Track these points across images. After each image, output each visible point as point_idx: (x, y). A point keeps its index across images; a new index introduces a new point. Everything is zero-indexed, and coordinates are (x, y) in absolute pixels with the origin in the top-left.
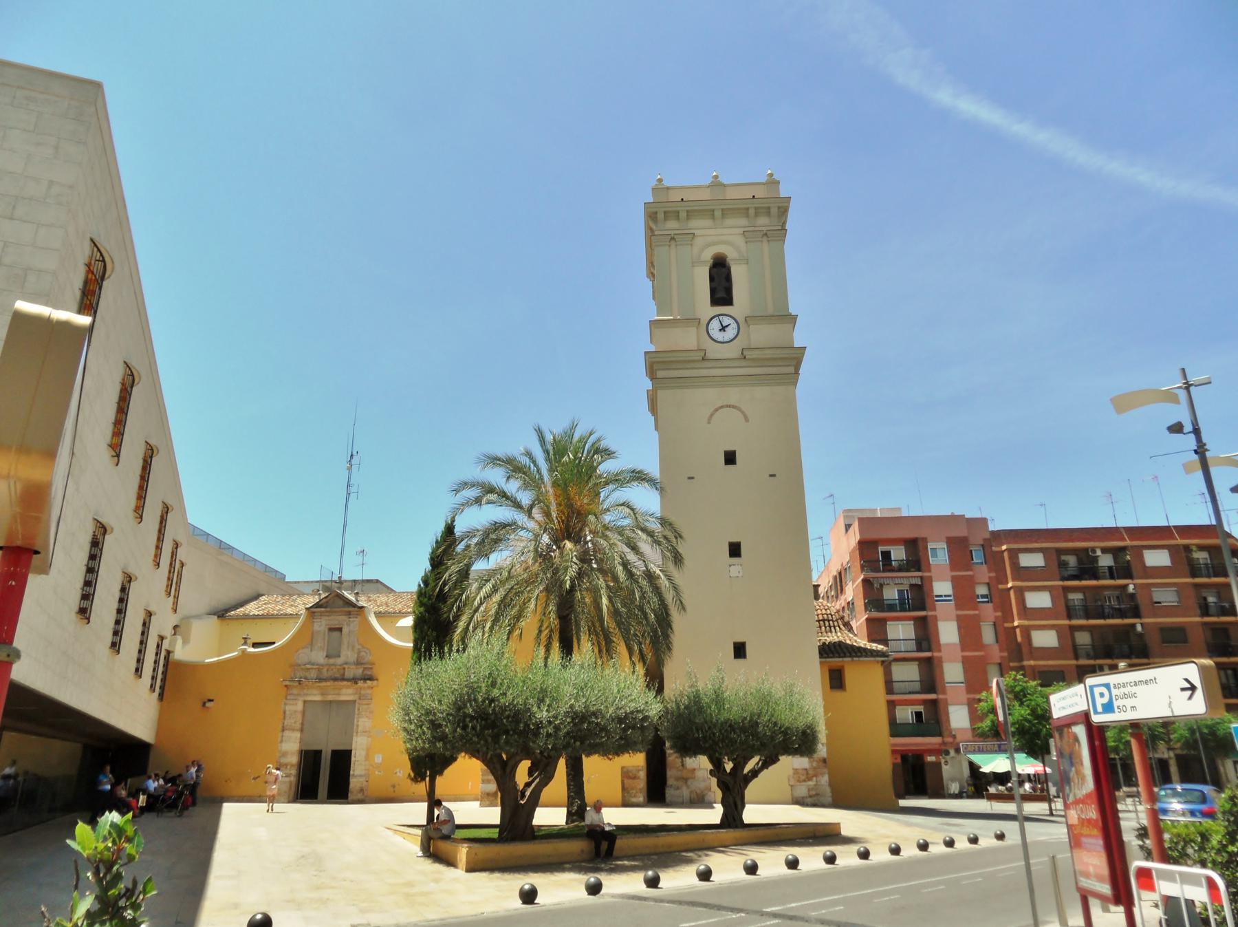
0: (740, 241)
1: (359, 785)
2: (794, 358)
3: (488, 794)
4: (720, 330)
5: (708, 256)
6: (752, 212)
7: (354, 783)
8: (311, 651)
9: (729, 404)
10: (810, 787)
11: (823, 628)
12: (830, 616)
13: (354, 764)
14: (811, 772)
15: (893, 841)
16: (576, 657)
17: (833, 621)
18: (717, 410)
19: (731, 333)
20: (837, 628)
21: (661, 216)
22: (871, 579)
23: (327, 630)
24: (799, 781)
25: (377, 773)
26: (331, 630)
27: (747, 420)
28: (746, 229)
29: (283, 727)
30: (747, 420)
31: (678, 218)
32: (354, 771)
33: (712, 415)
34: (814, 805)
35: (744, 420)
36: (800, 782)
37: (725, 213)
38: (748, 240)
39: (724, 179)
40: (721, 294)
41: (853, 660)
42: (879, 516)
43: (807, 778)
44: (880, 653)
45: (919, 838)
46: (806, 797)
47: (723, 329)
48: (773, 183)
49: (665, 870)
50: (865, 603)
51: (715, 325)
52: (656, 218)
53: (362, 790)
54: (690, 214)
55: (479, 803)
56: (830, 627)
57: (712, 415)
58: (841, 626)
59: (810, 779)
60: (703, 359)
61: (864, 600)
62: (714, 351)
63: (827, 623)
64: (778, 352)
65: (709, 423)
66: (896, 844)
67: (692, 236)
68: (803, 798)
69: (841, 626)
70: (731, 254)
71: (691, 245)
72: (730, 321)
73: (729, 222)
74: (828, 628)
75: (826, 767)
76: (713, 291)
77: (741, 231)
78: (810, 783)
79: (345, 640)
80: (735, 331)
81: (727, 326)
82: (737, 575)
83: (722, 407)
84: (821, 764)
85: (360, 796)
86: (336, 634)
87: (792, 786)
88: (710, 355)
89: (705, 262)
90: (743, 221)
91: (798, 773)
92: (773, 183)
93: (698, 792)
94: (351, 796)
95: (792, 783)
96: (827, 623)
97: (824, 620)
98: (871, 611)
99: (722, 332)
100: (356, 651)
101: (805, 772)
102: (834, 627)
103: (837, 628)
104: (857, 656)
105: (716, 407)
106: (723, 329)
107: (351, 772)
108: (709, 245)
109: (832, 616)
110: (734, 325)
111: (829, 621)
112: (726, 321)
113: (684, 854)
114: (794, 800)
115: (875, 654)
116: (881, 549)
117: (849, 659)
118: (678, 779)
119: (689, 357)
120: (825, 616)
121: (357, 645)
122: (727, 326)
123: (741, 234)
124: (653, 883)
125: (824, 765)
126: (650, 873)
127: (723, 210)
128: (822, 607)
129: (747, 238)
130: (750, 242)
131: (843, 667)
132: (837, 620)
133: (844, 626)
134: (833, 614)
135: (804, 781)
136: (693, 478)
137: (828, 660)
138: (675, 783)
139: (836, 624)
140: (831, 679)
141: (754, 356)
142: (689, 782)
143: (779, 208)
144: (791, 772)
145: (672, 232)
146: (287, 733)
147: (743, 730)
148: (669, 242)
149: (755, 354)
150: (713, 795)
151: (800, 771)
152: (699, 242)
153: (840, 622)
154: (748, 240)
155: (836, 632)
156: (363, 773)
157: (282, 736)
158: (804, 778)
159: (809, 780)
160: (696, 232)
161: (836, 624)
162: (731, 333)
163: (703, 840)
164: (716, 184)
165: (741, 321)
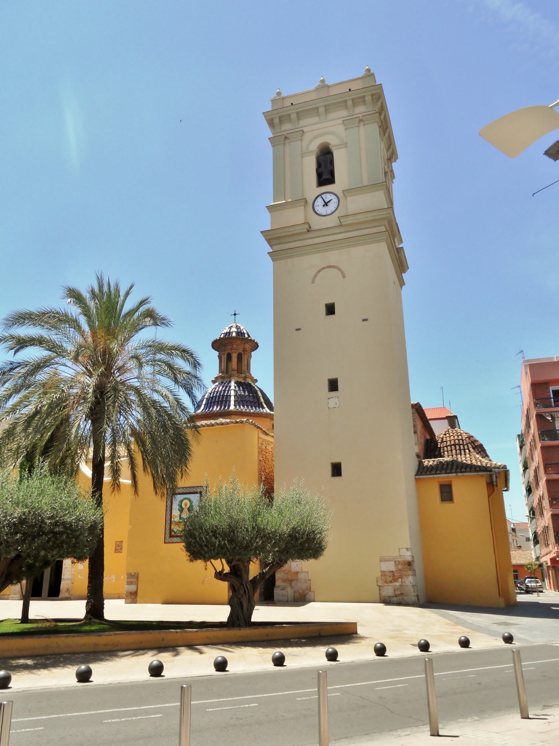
0: (340, 129)
1: (66, 586)
2: (383, 219)
3: (131, 593)
4: (324, 206)
5: (315, 146)
6: (350, 103)
7: (64, 585)
9: (329, 265)
10: (396, 588)
11: (454, 451)
12: (461, 441)
13: (64, 570)
14: (397, 574)
15: (422, 637)
16: (37, 471)
17: (464, 445)
18: (319, 271)
19: (332, 206)
20: (467, 451)
21: (276, 121)
22: (544, 414)
24: (386, 582)
25: (79, 577)
27: (344, 277)
28: (344, 119)
30: (344, 277)
31: (290, 121)
32: (64, 576)
33: (315, 276)
34: (399, 604)
35: (341, 276)
36: (387, 583)
37: (328, 109)
38: (346, 127)
39: (328, 82)
40: (326, 176)
41: (457, 476)
42: (556, 361)
43: (393, 579)
44: (482, 469)
45: (460, 636)
46: (393, 596)
47: (326, 204)
48: (369, 75)
49: (100, 662)
50: (539, 434)
51: (320, 202)
52: (273, 123)
53: (68, 590)
54: (300, 115)
55: (124, 600)
56: (460, 450)
57: (315, 276)
58: (471, 449)
59: (395, 580)
60: (308, 231)
61: (538, 432)
62: (317, 223)
63: (458, 447)
64: (370, 215)
65: (313, 282)
66: (425, 640)
67: (301, 132)
68: (389, 597)
69: (471, 449)
70: (332, 141)
71: (301, 140)
72: (333, 197)
73: (332, 116)
74: (458, 451)
75: (410, 569)
76: (319, 175)
77: (340, 121)
78: (397, 584)
80: (336, 205)
81: (329, 201)
82: (335, 406)
83: (324, 268)
84: (406, 566)
85: (67, 595)
87: (380, 586)
88: (314, 227)
89: (312, 151)
90: (343, 113)
91: (385, 575)
92: (369, 75)
93: (301, 591)
94: (61, 596)
95: (379, 584)
96: (458, 447)
97: (455, 445)
98: (544, 440)
99: (326, 208)
101: (391, 574)
102: (464, 450)
103: (467, 451)
104: (461, 472)
105: (319, 269)
106: (326, 204)
107: (62, 577)
108: (315, 138)
109: (463, 440)
110: (335, 200)
111: (459, 445)
112: (328, 197)
113: (195, 647)
114: (382, 599)
115: (478, 469)
116: (552, 388)
117: (454, 475)
118: (284, 581)
119: (295, 230)
120: (457, 441)
122: (329, 201)
123: (342, 123)
124: (84, 677)
125: (409, 567)
126: (83, 667)
127: (325, 106)
128: (455, 434)
129: (346, 126)
130: (349, 128)
131: (451, 481)
132: (467, 444)
133: (473, 448)
134: (464, 439)
135: (391, 582)
136: (364, 320)
137: (435, 476)
138: (282, 584)
139: (466, 447)
140: (442, 492)
141: (349, 222)
142: (293, 584)
143: (372, 95)
144: (379, 575)
145: (285, 133)
147: (225, 535)
148: (284, 141)
149: (349, 220)
150: (312, 595)
151: (387, 573)
152: (307, 137)
153: (470, 445)
154: (346, 127)
155: (465, 454)
156: (69, 577)
158: (390, 579)
159: (395, 581)
160: (305, 129)
161: (466, 447)
162: (332, 206)
163: (163, 639)
164: (323, 86)
165: (340, 194)
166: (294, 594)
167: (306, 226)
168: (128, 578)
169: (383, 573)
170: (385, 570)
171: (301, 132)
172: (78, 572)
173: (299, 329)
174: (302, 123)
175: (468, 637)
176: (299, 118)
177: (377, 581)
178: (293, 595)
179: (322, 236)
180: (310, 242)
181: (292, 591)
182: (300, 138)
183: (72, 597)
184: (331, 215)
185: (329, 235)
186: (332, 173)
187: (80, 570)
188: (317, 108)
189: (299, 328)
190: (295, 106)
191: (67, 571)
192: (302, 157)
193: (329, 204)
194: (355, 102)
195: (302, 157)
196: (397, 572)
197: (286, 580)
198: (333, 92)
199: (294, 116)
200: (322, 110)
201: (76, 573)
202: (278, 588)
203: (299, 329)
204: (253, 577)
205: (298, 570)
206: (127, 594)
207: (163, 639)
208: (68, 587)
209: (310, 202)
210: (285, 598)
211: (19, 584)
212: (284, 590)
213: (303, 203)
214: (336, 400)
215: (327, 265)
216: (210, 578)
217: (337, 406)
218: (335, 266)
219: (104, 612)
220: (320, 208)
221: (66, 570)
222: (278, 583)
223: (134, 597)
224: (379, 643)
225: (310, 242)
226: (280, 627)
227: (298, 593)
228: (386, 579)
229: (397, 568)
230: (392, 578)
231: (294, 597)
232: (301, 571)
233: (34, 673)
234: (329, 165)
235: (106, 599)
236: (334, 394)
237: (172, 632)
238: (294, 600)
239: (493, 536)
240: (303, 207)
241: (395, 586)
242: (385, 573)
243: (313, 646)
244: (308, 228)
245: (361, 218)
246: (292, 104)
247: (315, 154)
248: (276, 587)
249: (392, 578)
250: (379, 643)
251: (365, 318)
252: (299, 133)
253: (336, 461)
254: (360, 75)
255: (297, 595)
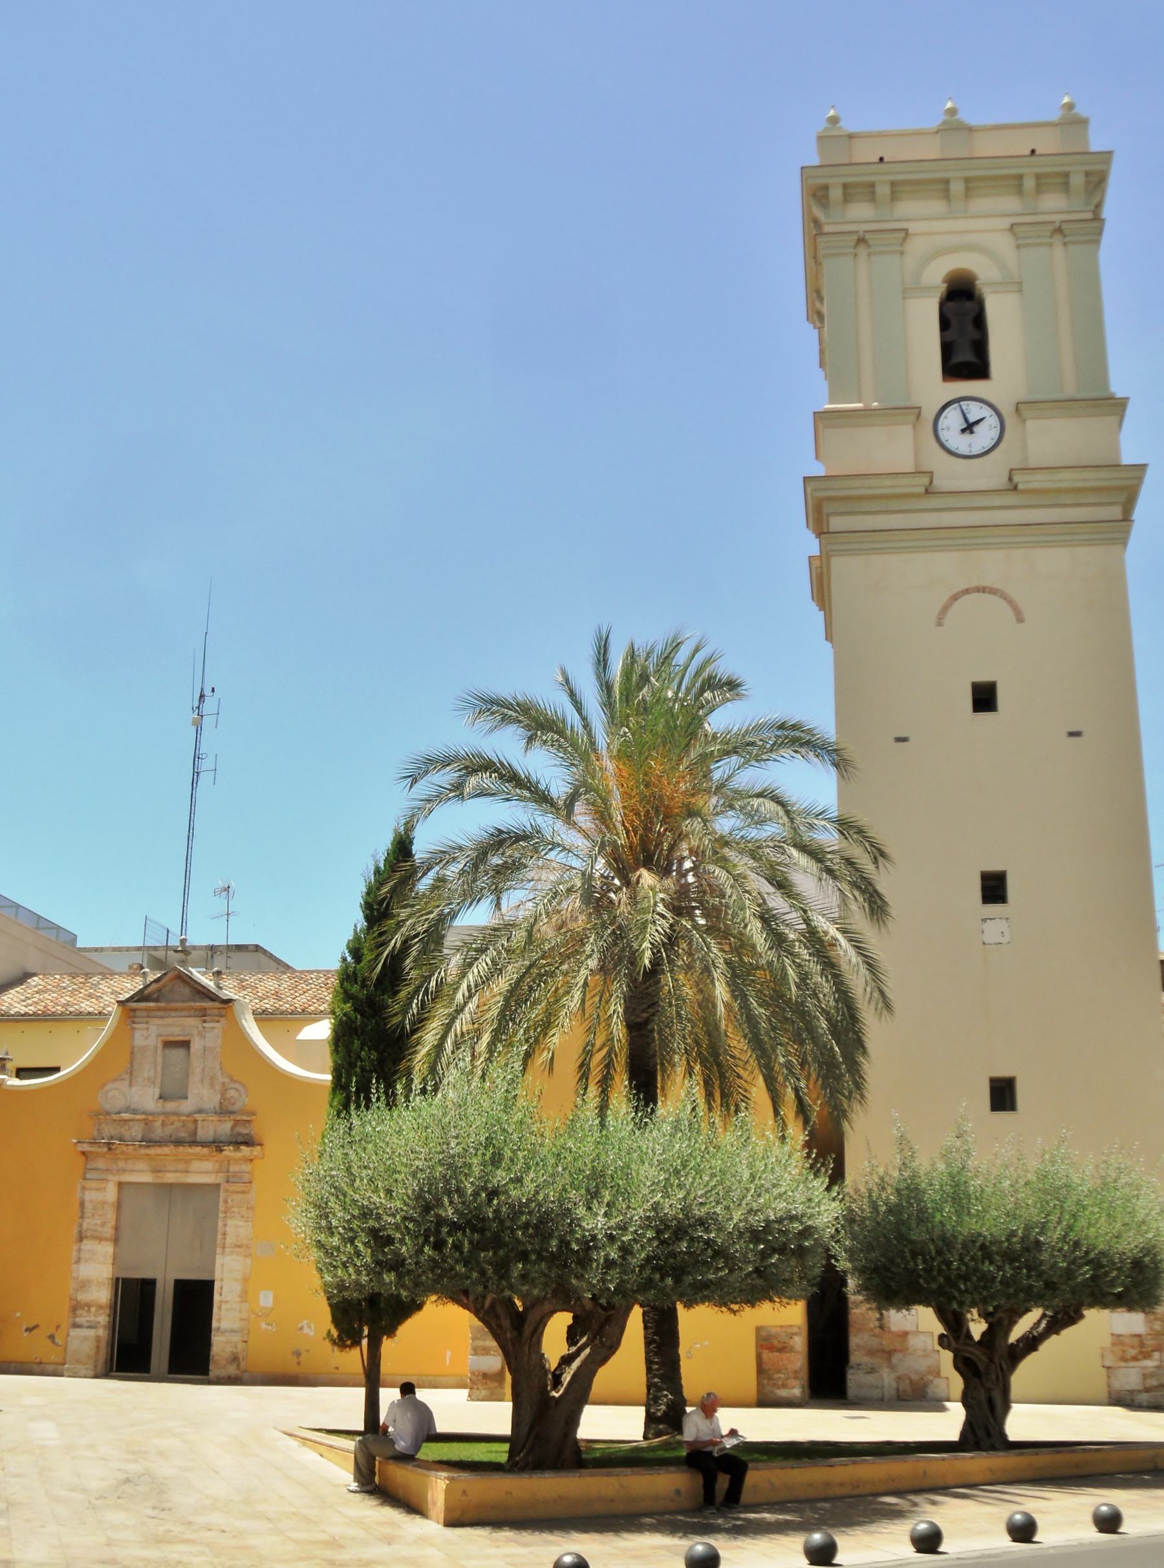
0: (1004, 244)
3: (485, 1376)
4: (963, 431)
5: (936, 276)
6: (1029, 183)
8: (131, 1085)
10: (1148, 1371)
13: (220, 1308)
19: (985, 435)
23: (160, 1046)
25: (264, 1326)
26: (168, 1044)
27: (1020, 619)
29: (80, 1232)
30: (1020, 619)
32: (219, 1320)
33: (945, 609)
36: (1126, 1361)
37: (971, 186)
39: (969, 117)
40: (965, 355)
43: (1141, 1352)
46: (1139, 1391)
47: (969, 428)
51: (952, 420)
53: (235, 1359)
55: (465, 1392)
57: (945, 609)
59: (1147, 1356)
60: (927, 491)
65: (939, 623)
71: (902, 253)
72: (986, 412)
73: (981, 204)
77: (1006, 222)
78: (1149, 1364)
79: (197, 1066)
80: (995, 433)
81: (978, 422)
83: (967, 591)
85: (232, 1370)
86: (178, 1054)
87: (1108, 1368)
88: (941, 483)
89: (930, 288)
90: (1010, 203)
91: (1122, 1344)
93: (914, 1377)
94: (214, 1371)
95: (1108, 1363)
99: (967, 437)
100: (218, 1087)
101: (1136, 1341)
106: (969, 428)
107: (214, 1324)
110: (992, 421)
112: (975, 411)
121: (219, 1074)
122: (978, 422)
129: (1018, 239)
130: (1027, 246)
135: (1135, 1359)
144: (1107, 1342)
145: (861, 228)
146: (87, 1245)
151: (1127, 1340)
152: (916, 247)
154: (1021, 242)
157: (79, 1250)
160: (913, 227)
162: (985, 435)
163: (925, 1473)
165: (1007, 410)
166: (897, 1383)
167: (925, 480)
168: (474, 1339)
169: (1117, 1339)
170: (1123, 1333)
172: (260, 1314)
173: (904, 740)
175: (1036, 1517)
176: (894, 196)
177: (1103, 1356)
178: (894, 1385)
180: (931, 519)
181: (893, 1376)
182: (899, 248)
183: (246, 1376)
184: (981, 460)
186: (980, 347)
187: (264, 1308)
189: (905, 735)
190: (887, 165)
191: (228, 1310)
192: (904, 298)
193: (976, 429)
194: (1043, 183)
195: (904, 298)
196: (1150, 1337)
197: (877, 1350)
198: (986, 147)
199: (883, 191)
200: (957, 187)
201: (253, 1316)
202: (858, 1369)
203: (904, 740)
204: (566, 1329)
205: (908, 1329)
206: (473, 1377)
207: (925, 1473)
208: (235, 1351)
209: (929, 414)
210: (876, 1393)
211: (358, 1348)
212: (873, 1375)
213: (913, 418)
214: (1004, 926)
215: (974, 583)
216: (706, 1343)
217: (1005, 940)
218: (998, 590)
221: (224, 1307)
222: (856, 1357)
223: (496, 1384)
224: (1105, 1504)
225: (931, 519)
226: (1070, 1452)
227: (907, 1381)
228: (1124, 1352)
229: (1151, 1329)
230: (1139, 1350)
231: (898, 1389)
232: (914, 1329)
233: (621, 1537)
234: (970, 328)
235: (385, 1386)
236: (994, 909)
237: (964, 1458)
238: (899, 1396)
240: (909, 428)
241: (1144, 1368)
242: (1121, 1338)
243: (613, 1531)
245: (1067, 479)
246: (881, 159)
248: (852, 1367)
249: (1139, 1350)
250: (1105, 1504)
251: (1074, 729)
252: (897, 235)
253: (1003, 1072)
255: (905, 1386)
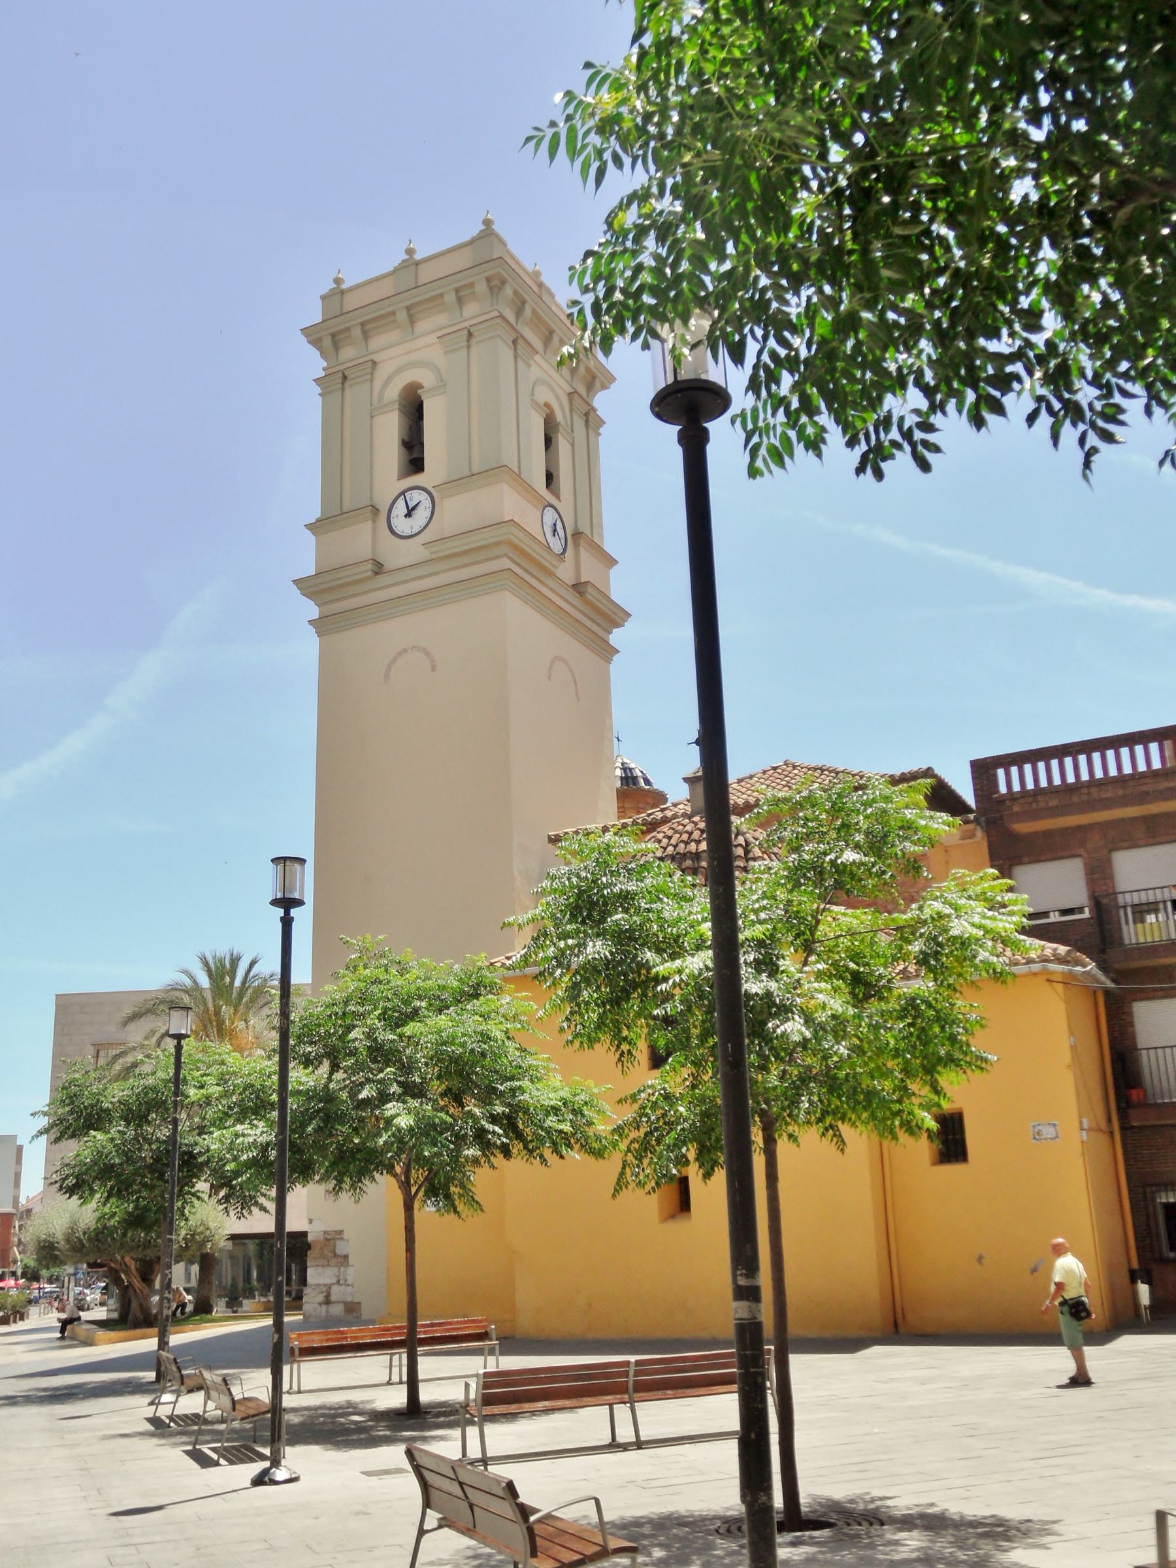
0: (436, 355)
5: (394, 392)
19: (422, 515)
27: (434, 669)
30: (434, 669)
51: (400, 508)
62: (397, 554)
70: (425, 378)
71: (372, 381)
80: (428, 513)
112: (416, 497)
143: (488, 280)
164: (411, 264)
171: (370, 364)
174: (376, 342)
179: (489, 559)
185: (407, 581)
188: (393, 313)
219: (380, 1449)
220: (402, 525)
239: (1121, 1206)
240: (370, 523)
244: (376, 569)
247: (397, 406)
254: (466, 237)
